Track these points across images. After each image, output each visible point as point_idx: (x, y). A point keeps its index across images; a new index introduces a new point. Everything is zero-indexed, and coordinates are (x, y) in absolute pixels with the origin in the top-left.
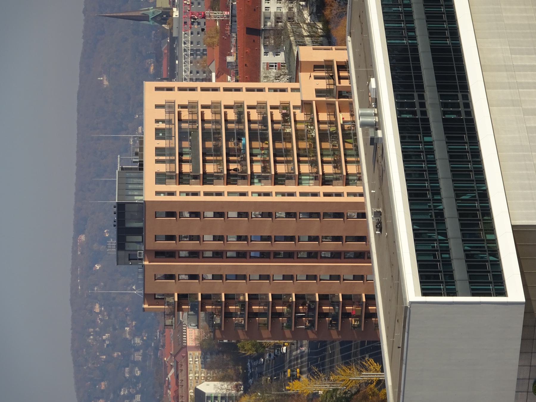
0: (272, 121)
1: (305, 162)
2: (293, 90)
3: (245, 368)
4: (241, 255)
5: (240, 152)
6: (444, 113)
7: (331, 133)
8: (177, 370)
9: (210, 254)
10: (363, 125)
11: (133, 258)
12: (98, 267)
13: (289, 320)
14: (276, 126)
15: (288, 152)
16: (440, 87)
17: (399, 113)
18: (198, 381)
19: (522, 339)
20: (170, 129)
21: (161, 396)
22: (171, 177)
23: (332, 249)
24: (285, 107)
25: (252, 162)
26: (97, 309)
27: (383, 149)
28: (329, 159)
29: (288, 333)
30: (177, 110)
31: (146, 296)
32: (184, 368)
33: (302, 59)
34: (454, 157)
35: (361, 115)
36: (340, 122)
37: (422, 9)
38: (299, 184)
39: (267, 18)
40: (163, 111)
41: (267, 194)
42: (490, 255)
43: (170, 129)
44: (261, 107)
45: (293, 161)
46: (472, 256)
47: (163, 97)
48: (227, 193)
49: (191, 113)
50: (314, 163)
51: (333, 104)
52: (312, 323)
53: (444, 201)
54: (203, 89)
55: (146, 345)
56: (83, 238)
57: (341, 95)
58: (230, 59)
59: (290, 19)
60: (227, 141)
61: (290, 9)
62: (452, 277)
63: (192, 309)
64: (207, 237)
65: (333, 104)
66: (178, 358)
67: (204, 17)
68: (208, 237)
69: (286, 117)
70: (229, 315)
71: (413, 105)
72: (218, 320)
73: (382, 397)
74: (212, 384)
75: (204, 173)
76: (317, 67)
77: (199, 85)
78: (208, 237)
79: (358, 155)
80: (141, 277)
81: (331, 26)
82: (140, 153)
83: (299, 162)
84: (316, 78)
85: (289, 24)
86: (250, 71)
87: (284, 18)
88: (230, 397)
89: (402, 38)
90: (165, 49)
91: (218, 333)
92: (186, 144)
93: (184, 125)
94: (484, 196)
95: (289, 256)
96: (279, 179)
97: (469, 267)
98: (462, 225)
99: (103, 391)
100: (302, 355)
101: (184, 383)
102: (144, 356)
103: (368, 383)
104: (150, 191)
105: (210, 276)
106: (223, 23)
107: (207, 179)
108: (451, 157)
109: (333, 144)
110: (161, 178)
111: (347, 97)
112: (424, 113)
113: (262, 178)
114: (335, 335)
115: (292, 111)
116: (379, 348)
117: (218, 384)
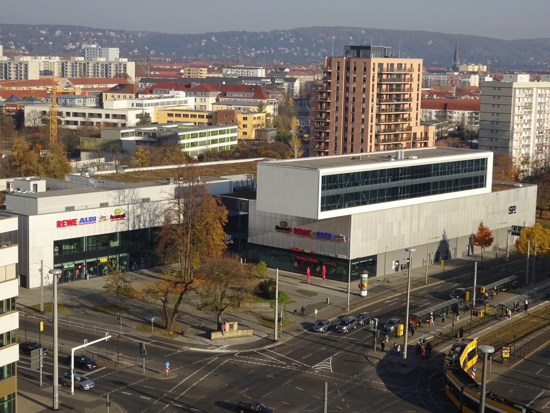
1: (385, 127)
2: (417, 123)
3: (304, 100)
4: (347, 99)
5: (391, 100)
6: (401, 188)
8: (306, 71)
10: (397, 153)
11: (347, 52)
12: (351, 38)
13: (319, 119)
14: (401, 115)
15: (390, 120)
18: (301, 79)
21: (296, 64)
22: (381, 70)
23: (348, 138)
24: (410, 119)
25: (386, 105)
28: (386, 138)
30: (410, 73)
31: (331, 58)
33: (430, 127)
34: (382, 191)
35: (401, 152)
36: (402, 143)
37: (460, 178)
38: (376, 125)
39: (451, 112)
40: (410, 67)
44: (410, 109)
47: (416, 67)
48: (373, 93)
49: (408, 79)
50: (385, 131)
51: (410, 140)
52: (317, 128)
54: (418, 84)
56: (364, 32)
57: (413, 143)
58: (435, 96)
62: (330, 189)
67: (453, 86)
68: (355, 85)
69: (405, 120)
70: (321, 93)
71: (405, 174)
72: (319, 88)
73: (287, 157)
74: (299, 86)
75: (382, 84)
76: (426, 134)
78: (355, 85)
79: (388, 150)
82: (392, 57)
83: (386, 125)
84: (421, 133)
86: (425, 105)
87: (450, 120)
88: (293, 93)
92: (395, 76)
94: (364, 203)
95: (346, 119)
96: (378, 116)
97: (334, 196)
98: (352, 194)
102: (313, 57)
103: (293, 151)
104: (375, 61)
105: (338, 86)
106: (450, 94)
107: (380, 85)
108: (382, 190)
109: (392, 139)
110: (380, 65)
112: (401, 179)
113: (379, 109)
117: (299, 88)
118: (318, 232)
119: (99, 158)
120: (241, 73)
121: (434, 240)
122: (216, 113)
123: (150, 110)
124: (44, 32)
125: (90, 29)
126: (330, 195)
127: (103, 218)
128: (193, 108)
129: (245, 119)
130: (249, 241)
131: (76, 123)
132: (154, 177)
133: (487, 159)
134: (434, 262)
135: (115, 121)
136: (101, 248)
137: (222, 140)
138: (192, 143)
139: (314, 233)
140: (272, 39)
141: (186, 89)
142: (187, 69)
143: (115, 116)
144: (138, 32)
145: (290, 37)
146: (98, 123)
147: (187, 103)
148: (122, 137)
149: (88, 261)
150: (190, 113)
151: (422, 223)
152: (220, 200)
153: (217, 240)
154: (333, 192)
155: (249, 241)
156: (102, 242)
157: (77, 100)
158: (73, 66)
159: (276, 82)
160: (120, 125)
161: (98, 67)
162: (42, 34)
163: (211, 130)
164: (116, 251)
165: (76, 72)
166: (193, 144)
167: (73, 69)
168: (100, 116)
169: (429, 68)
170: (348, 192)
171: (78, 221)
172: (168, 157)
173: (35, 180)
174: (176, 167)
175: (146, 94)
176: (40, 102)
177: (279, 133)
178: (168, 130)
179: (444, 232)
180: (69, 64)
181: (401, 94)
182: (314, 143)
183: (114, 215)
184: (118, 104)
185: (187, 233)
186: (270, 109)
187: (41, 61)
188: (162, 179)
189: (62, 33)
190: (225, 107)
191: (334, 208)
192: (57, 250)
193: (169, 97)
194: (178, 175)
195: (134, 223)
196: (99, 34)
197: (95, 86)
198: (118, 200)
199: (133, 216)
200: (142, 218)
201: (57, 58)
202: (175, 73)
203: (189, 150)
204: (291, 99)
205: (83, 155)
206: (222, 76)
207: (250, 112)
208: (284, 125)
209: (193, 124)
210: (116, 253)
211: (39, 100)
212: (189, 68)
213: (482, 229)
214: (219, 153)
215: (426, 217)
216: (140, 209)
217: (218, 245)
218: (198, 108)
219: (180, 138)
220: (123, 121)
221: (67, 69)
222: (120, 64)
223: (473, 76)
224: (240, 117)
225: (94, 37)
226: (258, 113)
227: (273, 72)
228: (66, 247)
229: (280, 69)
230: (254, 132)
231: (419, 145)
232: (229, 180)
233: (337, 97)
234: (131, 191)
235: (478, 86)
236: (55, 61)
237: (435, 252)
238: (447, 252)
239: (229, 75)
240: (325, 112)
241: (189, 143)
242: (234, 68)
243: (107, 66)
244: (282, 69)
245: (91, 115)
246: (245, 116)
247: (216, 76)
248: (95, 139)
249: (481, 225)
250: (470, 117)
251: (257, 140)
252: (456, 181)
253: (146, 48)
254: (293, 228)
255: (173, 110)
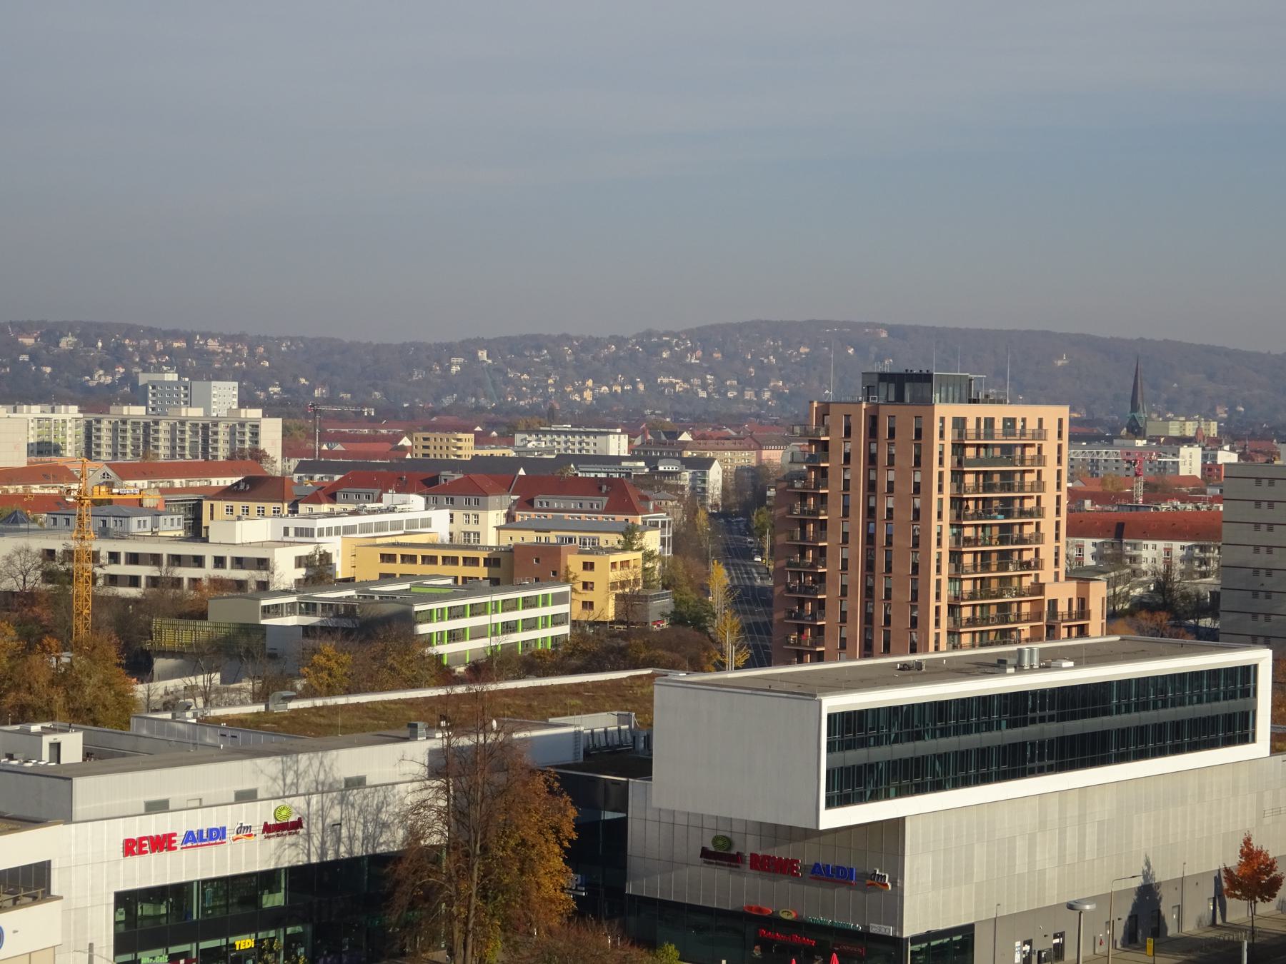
0: (1021, 550)
2: (1057, 574)
3: (737, 515)
4: (870, 512)
5: (987, 513)
6: (1032, 744)
7: (1007, 616)
9: (873, 477)
10: (1020, 652)
11: (869, 391)
12: (851, 351)
13: (797, 565)
14: (1016, 554)
16: (1062, 740)
17: (1034, 693)
19: (791, 827)
20: (1015, 435)
22: (960, 435)
23: (876, 615)
24: (1038, 564)
25: (976, 526)
26: (803, 350)
27: (992, 674)
28: (978, 614)
29: (782, 563)
30: (1037, 442)
31: (828, 404)
32: (738, 446)
33: (1092, 584)
34: (983, 754)
35: (1031, 650)
36: (1020, 626)
37: (1186, 717)
38: (950, 579)
41: (939, 543)
42: (872, 792)
43: (1015, 435)
44: (1038, 537)
45: (976, 572)
46: (871, 771)
47: (1051, 427)
48: (941, 497)
49: (1033, 459)
50: (973, 596)
51: (1040, 618)
52: (790, 591)
53: (934, 741)
54: (1059, 472)
55: (762, 404)
56: (884, 335)
57: (1051, 628)
58: (1088, 503)
59: (1134, 573)
60: (1001, 499)
61: (1145, 573)
62: (849, 748)
63: (811, 456)
64: (892, 474)
65: (1040, 619)
66: (748, 439)
67: (1137, 475)
68: (891, 476)
69: (1027, 566)
70: (803, 497)
71: (1042, 709)
72: (798, 485)
76: (1083, 602)
77: (1065, 468)
78: (891, 476)
79: (982, 645)
80: (849, 399)
81: (1128, 618)
82: (987, 400)
83: (975, 579)
84: (1070, 600)
85: (1128, 571)
86: (1078, 528)
87: (1135, 566)
88: (704, 498)
89: (1119, 699)
90: (1098, 430)
91: (785, 484)
92: (997, 452)
93: (1018, 450)
94: (938, 786)
95: (869, 566)
96: (956, 556)
97: (860, 767)
98: (906, 761)
99: (711, 355)
100: (752, 579)
101: (720, 446)
102: (750, 401)
104: (945, 411)
105: (847, 477)
106: (1130, 497)
107: (958, 475)
109: (996, 617)
111: (1048, 635)
112: (1033, 721)
113: (957, 537)
114: (778, 616)
115: (1033, 572)
116: (762, 664)
118: (817, 865)
119: (210, 672)
120: (577, 446)
121: (1124, 885)
122: (511, 551)
123: (334, 546)
124: (29, 341)
125: (151, 332)
126: (849, 763)
127: (244, 830)
128: (447, 540)
129: (588, 566)
130: (629, 890)
131: (134, 581)
132: (369, 721)
133: (1256, 666)
134: (1123, 945)
135: (241, 574)
136: (237, 911)
137: (530, 624)
138: (450, 632)
139: (805, 868)
140: (641, 355)
141: (426, 489)
142: (420, 435)
143: (239, 562)
144: (281, 339)
145: (687, 350)
146: (195, 582)
147: (429, 526)
148: (264, 618)
149: (204, 945)
150: (440, 554)
151: (1091, 839)
152: (556, 779)
153: (549, 889)
154: (856, 757)
155: (629, 890)
156: (239, 894)
157: (134, 521)
158: (115, 430)
159: (661, 468)
160: (253, 586)
161: (183, 432)
162: (24, 345)
163: (500, 597)
164: (276, 918)
165: (124, 446)
166: (460, 632)
167: (115, 438)
168: (198, 561)
169: (1081, 434)
170: (896, 757)
171: (179, 840)
172: (392, 669)
173: (53, 730)
174: (442, 692)
175: (320, 502)
176: (35, 526)
177: (677, 603)
178: (386, 598)
179: (1148, 863)
180: (105, 425)
181: (1014, 498)
182: (780, 627)
183: (272, 822)
184: (249, 530)
185: (470, 868)
186: (652, 540)
187: (30, 417)
188: (389, 728)
189: (76, 344)
190: (530, 537)
191: (860, 799)
192: (122, 918)
193: (381, 511)
194: (443, 715)
195: (323, 843)
196: (176, 345)
197: (178, 483)
198: (281, 782)
199: (320, 826)
200: (344, 832)
201: (74, 409)
202: (387, 447)
203: (446, 649)
204: (702, 515)
205: (160, 664)
206: (513, 454)
207: (597, 550)
208: (691, 581)
209: (450, 581)
210: (275, 925)
211: (35, 520)
212: (426, 434)
213: (1250, 854)
214: (520, 658)
215: (1101, 823)
216: (338, 808)
217: (552, 901)
218: (459, 539)
219: (419, 618)
220: (262, 575)
221: (99, 438)
222: (242, 425)
223: (1185, 450)
224: (574, 562)
225: (162, 353)
226: (624, 550)
227: (649, 443)
228: (145, 910)
229: (666, 434)
230: (612, 603)
231: (1064, 632)
232: (571, 730)
233: (846, 508)
234: (316, 758)
235: (1199, 476)
236: (68, 417)
237: (1125, 917)
238: (1158, 918)
239: (531, 451)
240: (815, 548)
241: (442, 632)
242: (545, 433)
243: (206, 431)
244: (674, 435)
245: (177, 560)
246: (588, 558)
247: (498, 453)
248: (191, 622)
249: (1247, 842)
250: (1188, 559)
251: (622, 623)
252: (1177, 726)
253: (303, 381)
254: (748, 855)
255: (394, 545)
